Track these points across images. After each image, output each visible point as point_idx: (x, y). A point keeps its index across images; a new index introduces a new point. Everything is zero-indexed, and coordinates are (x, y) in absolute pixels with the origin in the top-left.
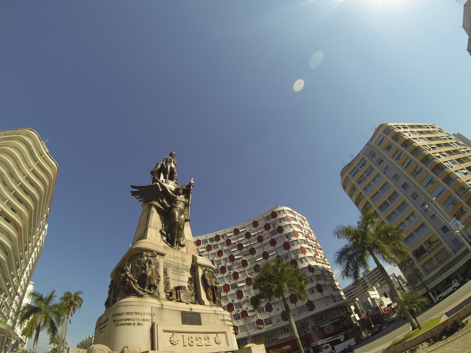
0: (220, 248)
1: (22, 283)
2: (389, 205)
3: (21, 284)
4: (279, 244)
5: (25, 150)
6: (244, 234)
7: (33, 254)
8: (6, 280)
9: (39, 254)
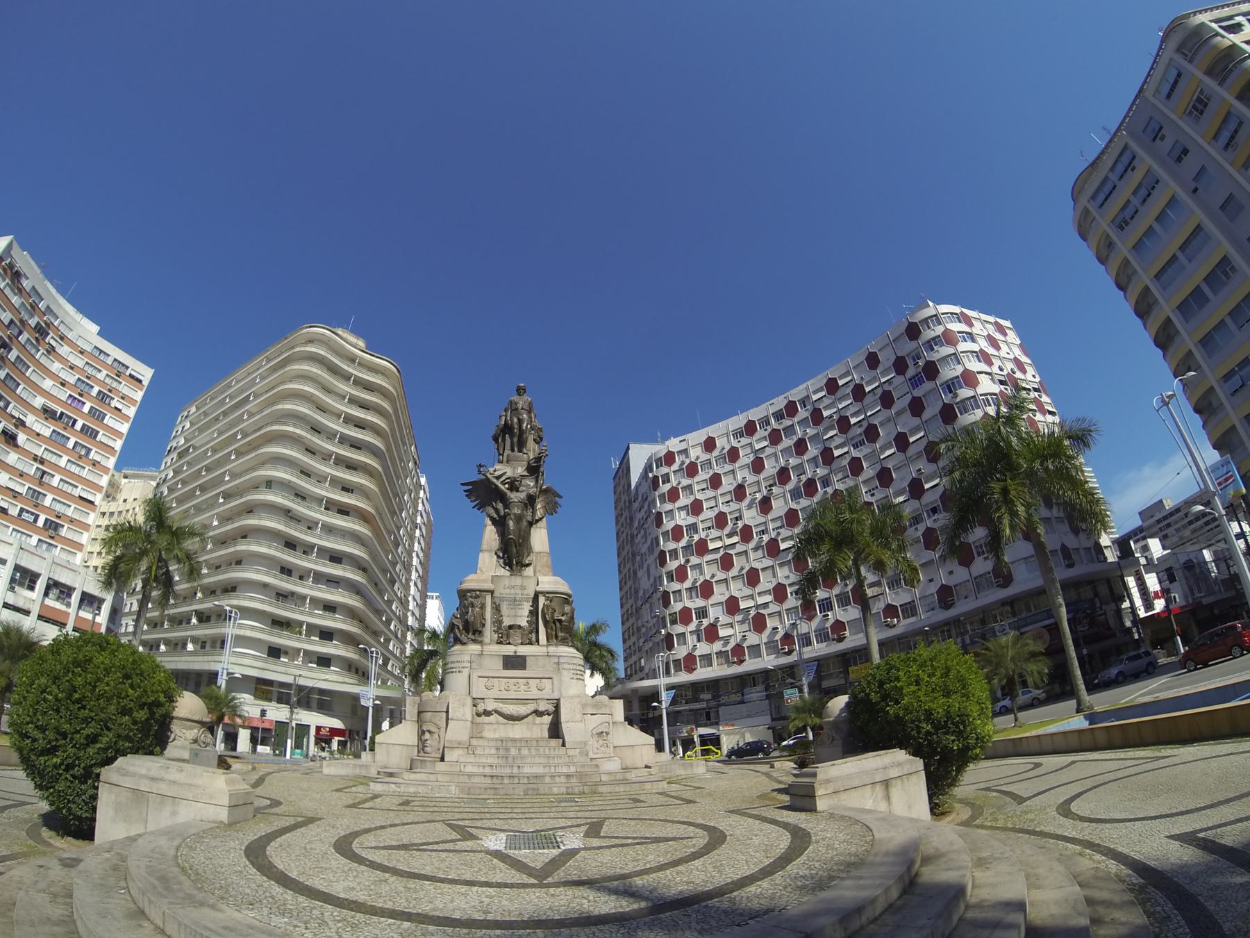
0: (799, 433)
1: (412, 605)
2: (1208, 300)
3: (411, 607)
4: (931, 410)
5: (319, 372)
6: (849, 390)
7: (416, 545)
8: (379, 613)
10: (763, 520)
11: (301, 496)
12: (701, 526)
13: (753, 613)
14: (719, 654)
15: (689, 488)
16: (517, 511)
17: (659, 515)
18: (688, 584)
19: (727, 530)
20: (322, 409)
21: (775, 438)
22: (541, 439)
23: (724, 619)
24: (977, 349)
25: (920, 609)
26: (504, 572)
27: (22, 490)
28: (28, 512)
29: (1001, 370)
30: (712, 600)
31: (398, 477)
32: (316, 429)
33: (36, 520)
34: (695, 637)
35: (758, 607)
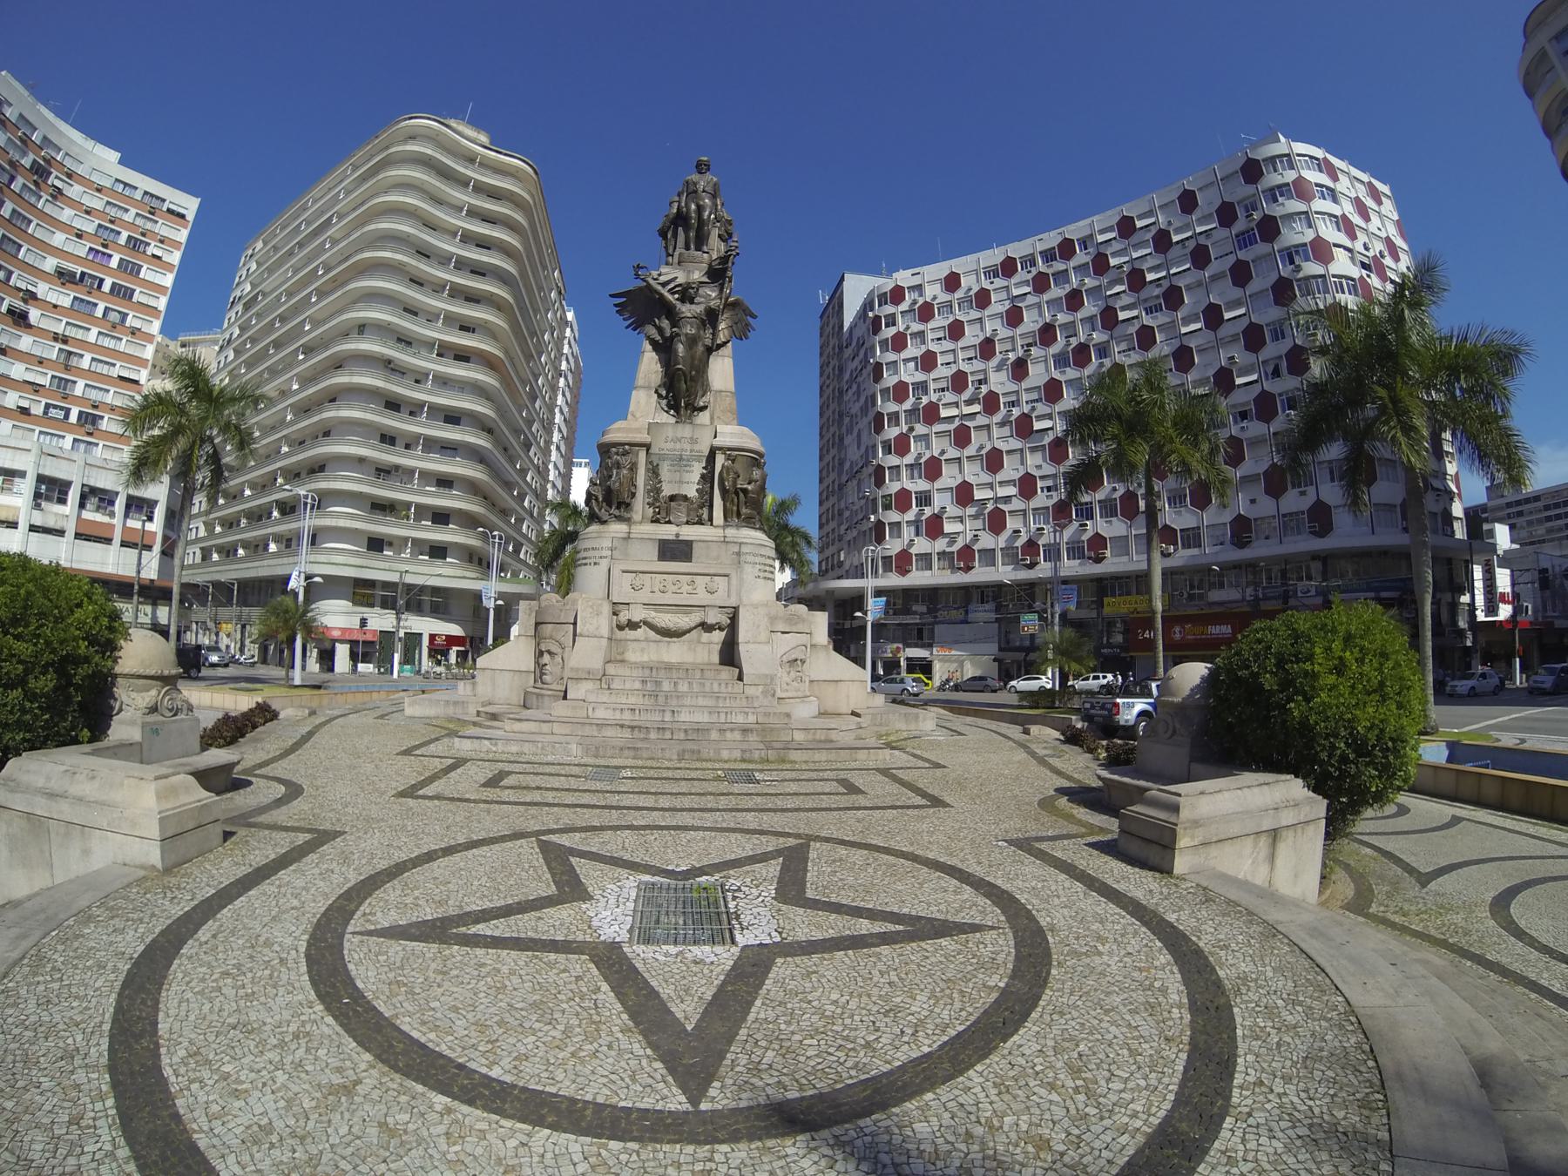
0: (1074, 281)
3: (551, 478)
4: (1261, 282)
6: (1149, 236)
7: (560, 397)
8: (508, 485)
9: (576, 391)
10: (1015, 388)
11: (405, 341)
12: (932, 386)
13: (990, 506)
14: (942, 555)
15: (920, 335)
16: (689, 330)
17: (878, 366)
18: (909, 459)
19: (966, 395)
20: (430, 225)
21: (1041, 283)
22: (730, 235)
23: (953, 510)
24: (1338, 213)
25: (1205, 540)
26: (667, 418)
27: (45, 381)
28: (55, 407)
29: (1367, 249)
30: (938, 484)
31: (536, 311)
32: (424, 253)
33: (67, 416)
34: (913, 529)
35: (997, 500)
